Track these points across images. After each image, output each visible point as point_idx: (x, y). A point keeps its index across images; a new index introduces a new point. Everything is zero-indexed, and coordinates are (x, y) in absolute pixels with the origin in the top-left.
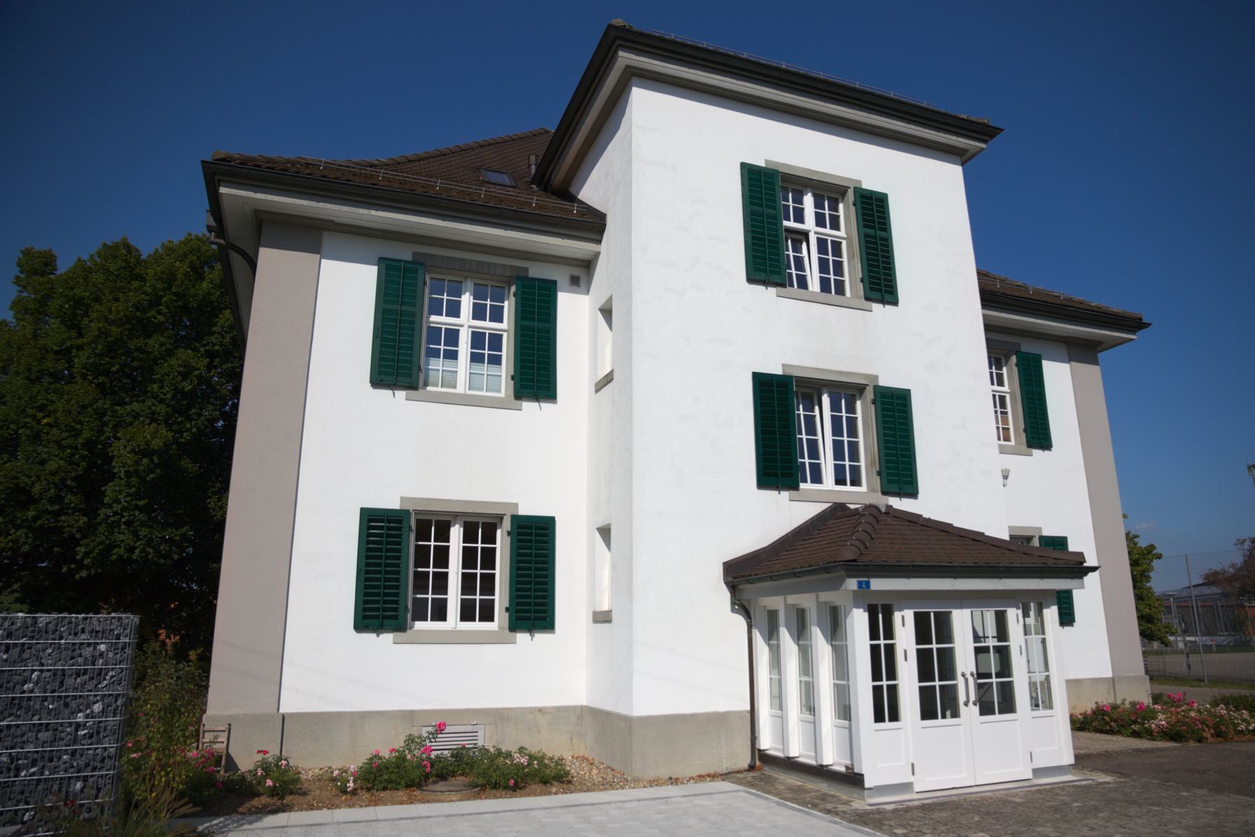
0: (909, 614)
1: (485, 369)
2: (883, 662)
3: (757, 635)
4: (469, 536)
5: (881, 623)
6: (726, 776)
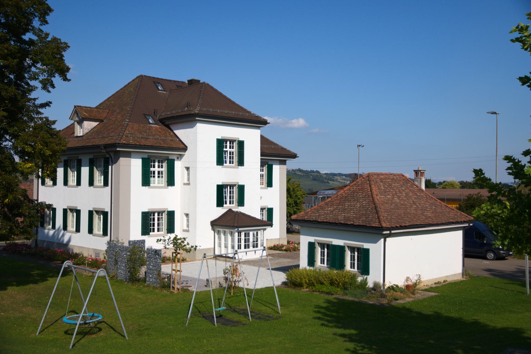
0: (243, 233)
2: (239, 241)
3: (216, 234)
4: (158, 215)
5: (239, 235)
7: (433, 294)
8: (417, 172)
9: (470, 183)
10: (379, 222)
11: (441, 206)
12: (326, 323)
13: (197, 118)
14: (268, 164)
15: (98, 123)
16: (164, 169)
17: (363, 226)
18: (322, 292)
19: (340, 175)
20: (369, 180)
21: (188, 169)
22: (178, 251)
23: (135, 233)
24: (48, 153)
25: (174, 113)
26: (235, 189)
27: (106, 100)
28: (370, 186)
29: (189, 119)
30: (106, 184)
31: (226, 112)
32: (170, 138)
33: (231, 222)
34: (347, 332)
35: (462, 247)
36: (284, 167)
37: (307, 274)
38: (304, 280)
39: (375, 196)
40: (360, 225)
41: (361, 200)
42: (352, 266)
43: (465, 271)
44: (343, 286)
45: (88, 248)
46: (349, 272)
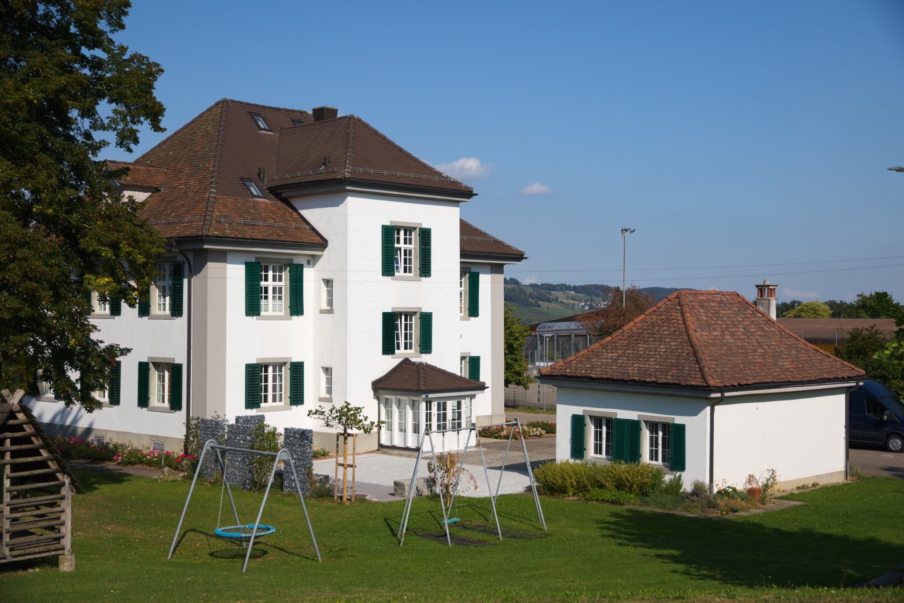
0: (436, 403)
1: (278, 302)
2: (429, 417)
5: (428, 407)
6: (372, 452)
7: (796, 503)
8: (761, 289)
9: (851, 306)
10: (703, 377)
11: (807, 350)
12: (624, 542)
13: (348, 188)
14: (470, 273)
15: (149, 194)
16: (284, 283)
17: (675, 384)
18: (602, 500)
19: (563, 288)
20: (679, 304)
21: (328, 282)
22: (349, 431)
23: (233, 406)
24: (141, 259)
25: (299, 176)
26: (415, 321)
27: (156, 147)
28: (683, 314)
29: (332, 188)
30: (176, 311)
31: (399, 175)
32: (294, 225)
33: (408, 383)
34: (661, 552)
35: (844, 424)
36: (500, 278)
37: (574, 471)
38: (569, 481)
39: (691, 332)
40: (668, 384)
41: (667, 340)
42: (654, 455)
43: (851, 468)
44: (641, 490)
45: (139, 434)
46: (648, 465)
